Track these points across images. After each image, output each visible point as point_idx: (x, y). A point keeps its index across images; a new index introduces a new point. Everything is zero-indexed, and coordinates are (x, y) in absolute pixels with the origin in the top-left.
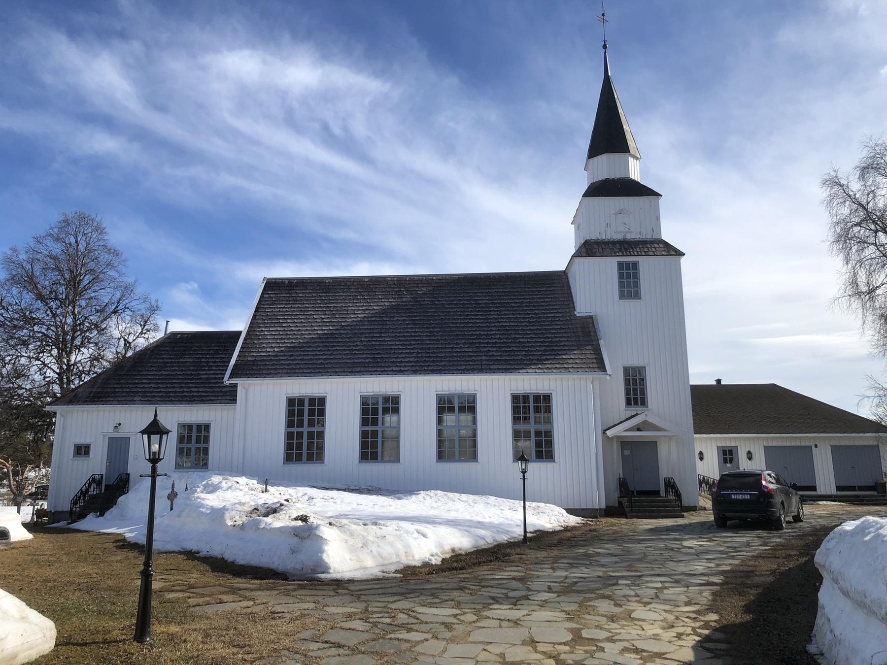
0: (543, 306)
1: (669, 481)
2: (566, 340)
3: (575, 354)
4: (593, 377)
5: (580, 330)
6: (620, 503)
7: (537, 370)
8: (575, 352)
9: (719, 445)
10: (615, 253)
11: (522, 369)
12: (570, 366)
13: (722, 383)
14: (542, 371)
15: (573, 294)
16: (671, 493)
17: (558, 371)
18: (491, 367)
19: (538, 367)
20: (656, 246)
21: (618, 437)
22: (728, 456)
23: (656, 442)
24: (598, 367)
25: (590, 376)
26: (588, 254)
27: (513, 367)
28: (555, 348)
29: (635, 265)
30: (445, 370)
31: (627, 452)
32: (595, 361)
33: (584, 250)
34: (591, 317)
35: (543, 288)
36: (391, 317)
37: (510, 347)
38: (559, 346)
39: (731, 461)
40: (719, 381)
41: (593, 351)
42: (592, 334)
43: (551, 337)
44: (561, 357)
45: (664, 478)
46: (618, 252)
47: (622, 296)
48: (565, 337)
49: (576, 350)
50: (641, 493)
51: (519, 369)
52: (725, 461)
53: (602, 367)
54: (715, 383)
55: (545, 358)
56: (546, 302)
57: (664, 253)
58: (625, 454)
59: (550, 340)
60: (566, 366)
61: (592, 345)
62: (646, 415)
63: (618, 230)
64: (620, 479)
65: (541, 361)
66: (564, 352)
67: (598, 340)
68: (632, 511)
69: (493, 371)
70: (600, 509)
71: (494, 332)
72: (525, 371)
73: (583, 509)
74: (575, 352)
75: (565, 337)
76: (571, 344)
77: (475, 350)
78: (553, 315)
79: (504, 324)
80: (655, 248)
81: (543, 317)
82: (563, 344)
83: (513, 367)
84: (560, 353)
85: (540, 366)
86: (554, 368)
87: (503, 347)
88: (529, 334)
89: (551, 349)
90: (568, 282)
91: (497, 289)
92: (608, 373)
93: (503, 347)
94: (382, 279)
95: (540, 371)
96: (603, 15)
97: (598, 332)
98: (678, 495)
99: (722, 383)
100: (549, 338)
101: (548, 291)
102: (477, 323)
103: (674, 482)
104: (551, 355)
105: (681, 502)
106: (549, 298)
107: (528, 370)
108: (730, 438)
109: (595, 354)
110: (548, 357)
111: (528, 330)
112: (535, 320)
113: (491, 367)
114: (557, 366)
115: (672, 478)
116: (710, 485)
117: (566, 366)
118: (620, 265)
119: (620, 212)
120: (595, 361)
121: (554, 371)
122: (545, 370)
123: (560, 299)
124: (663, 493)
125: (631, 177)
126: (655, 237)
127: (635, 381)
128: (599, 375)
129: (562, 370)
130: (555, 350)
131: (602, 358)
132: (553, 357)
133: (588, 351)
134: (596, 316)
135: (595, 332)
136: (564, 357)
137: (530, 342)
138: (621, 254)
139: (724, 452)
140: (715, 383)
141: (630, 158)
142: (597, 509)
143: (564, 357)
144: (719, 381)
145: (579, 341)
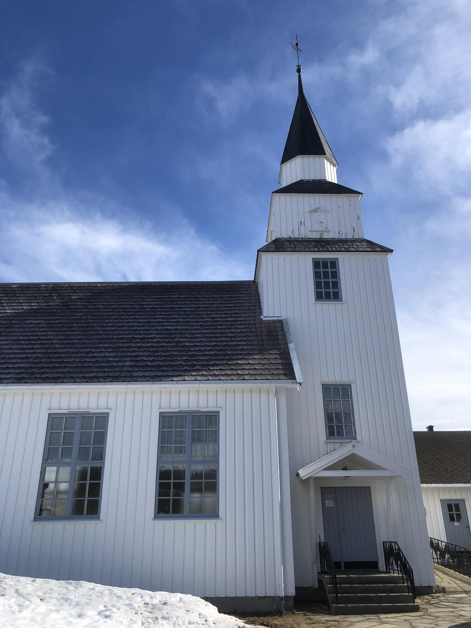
0: (223, 310)
1: (391, 547)
2: (245, 343)
3: (255, 360)
4: (276, 387)
5: (265, 333)
6: (320, 582)
7: (198, 378)
8: (255, 357)
9: (443, 497)
10: (309, 248)
11: (177, 376)
12: (247, 372)
13: (435, 429)
14: (206, 378)
15: (260, 293)
16: (395, 567)
17: (228, 378)
18: (134, 374)
19: (201, 373)
20: (358, 244)
21: (317, 480)
22: (454, 512)
23: (369, 488)
24: (284, 374)
25: (272, 385)
26: (277, 248)
27: (166, 374)
28: (229, 353)
29: (334, 264)
30: (65, 378)
31: (330, 503)
32: (280, 367)
33: (273, 246)
34: (281, 322)
35: (228, 294)
36: (22, 320)
37: (169, 351)
38: (235, 350)
39: (459, 517)
40: (431, 428)
41: (279, 356)
42: (281, 338)
43: (227, 341)
44: (235, 362)
45: (383, 543)
46: (313, 248)
47: (319, 297)
48: (245, 341)
49: (256, 354)
50: (352, 566)
51: (173, 376)
52: (452, 519)
53: (290, 374)
54: (426, 430)
55: (213, 363)
56: (228, 307)
57: (368, 249)
58: (327, 506)
59: (225, 343)
60: (239, 372)
61: (279, 349)
62: (354, 446)
63: (314, 229)
64: (320, 543)
65: (206, 367)
66: (241, 357)
67: (286, 344)
68: (337, 600)
69: (135, 379)
70: (286, 598)
71: (153, 336)
72: (182, 378)
73: (260, 598)
74: (255, 357)
75: (245, 341)
76: (251, 348)
77: (119, 354)
78: (233, 319)
79: (168, 327)
80: (357, 245)
81: (221, 321)
82: (241, 348)
83: (166, 374)
84: (234, 357)
85: (204, 373)
86: (223, 375)
87: (159, 351)
88: (199, 338)
89: (224, 353)
90: (257, 290)
91: (172, 295)
92: (298, 380)
93: (159, 351)
94: (34, 286)
95: (203, 378)
96: (297, 45)
97: (287, 335)
98: (407, 571)
99: (435, 429)
100: (224, 341)
101: (232, 297)
102: (134, 326)
103: (399, 549)
104: (223, 360)
105: (412, 581)
106: (232, 304)
107: (186, 378)
108: (455, 489)
109: (281, 359)
110: (217, 362)
111: (198, 334)
112: (210, 323)
113: (134, 374)
114: (228, 372)
115: (395, 543)
116: (441, 551)
117: (239, 372)
118: (316, 264)
119: (316, 210)
120: (280, 367)
121: (223, 378)
122: (210, 378)
123: (245, 305)
124: (382, 565)
125: (327, 179)
126: (356, 237)
127: (338, 415)
128: (286, 384)
129: (234, 378)
130: (229, 355)
131: (291, 364)
132: (224, 362)
133: (273, 356)
134: (286, 319)
135: (284, 336)
136: (239, 362)
137: (197, 346)
138: (316, 249)
139: (450, 507)
140: (426, 430)
141: (326, 161)
142: (281, 598)
143: (239, 362)
144: (431, 428)
145: (263, 345)
